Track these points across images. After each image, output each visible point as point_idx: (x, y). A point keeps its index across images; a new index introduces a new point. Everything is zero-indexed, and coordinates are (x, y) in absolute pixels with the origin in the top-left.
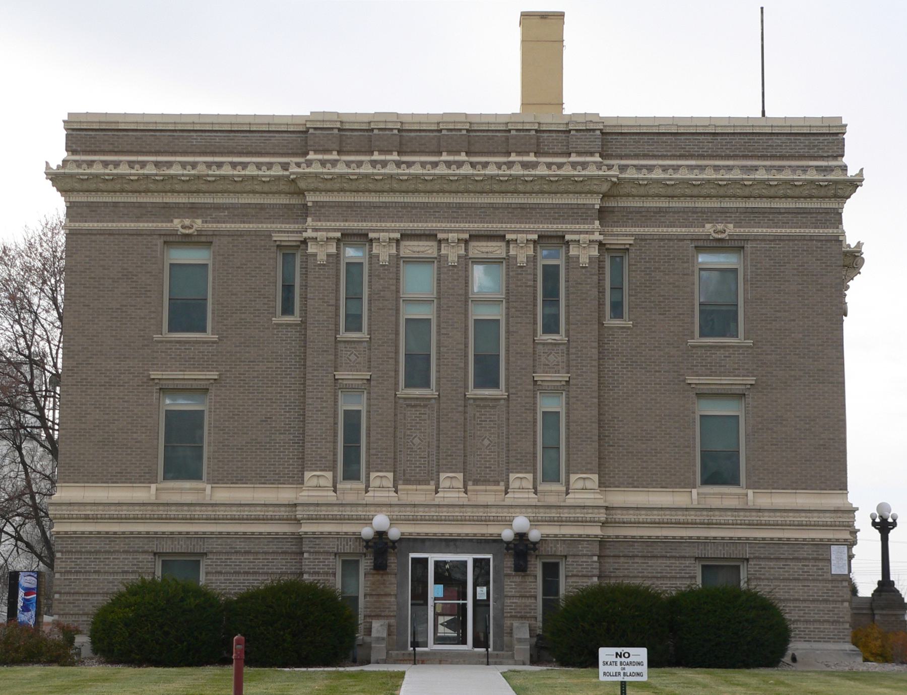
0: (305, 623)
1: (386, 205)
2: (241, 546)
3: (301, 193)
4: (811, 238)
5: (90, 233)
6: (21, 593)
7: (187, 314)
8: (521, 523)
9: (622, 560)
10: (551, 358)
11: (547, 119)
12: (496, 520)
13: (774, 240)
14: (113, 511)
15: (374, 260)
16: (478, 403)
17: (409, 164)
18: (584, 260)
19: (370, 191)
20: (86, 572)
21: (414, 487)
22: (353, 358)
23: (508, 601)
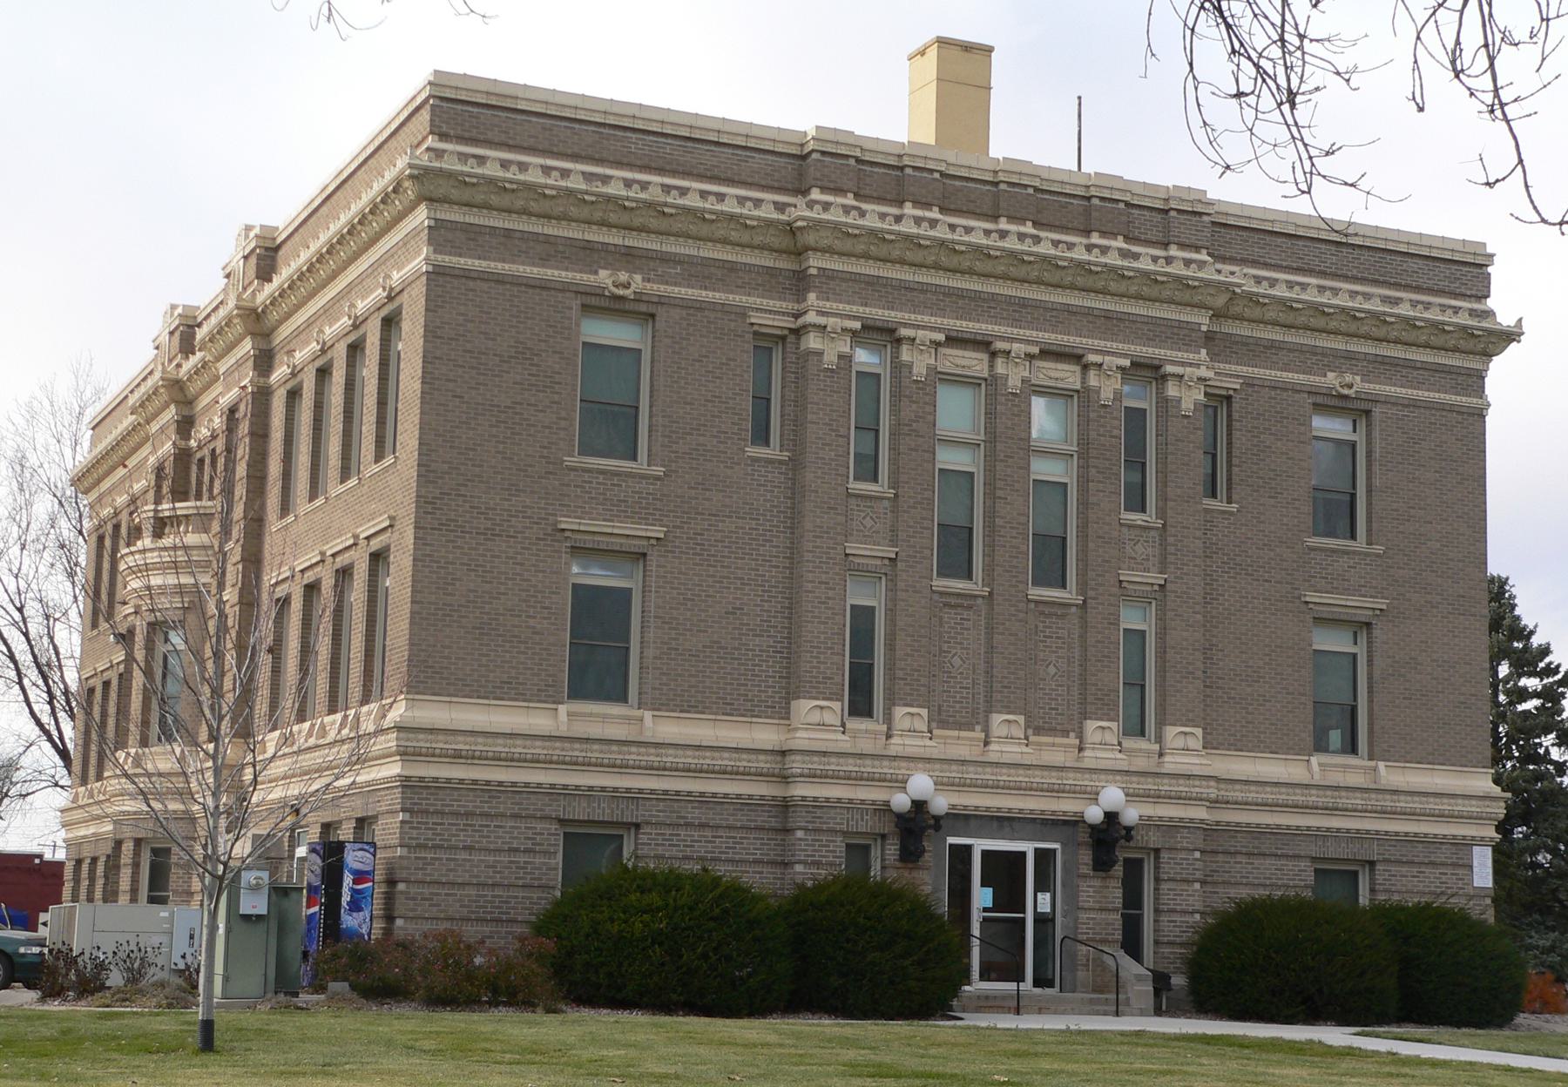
0: (865, 940)
1: (923, 289)
2: (693, 814)
3: (799, 253)
4: (1451, 409)
5: (466, 275)
6: (348, 879)
7: (612, 425)
8: (1112, 796)
9: (1221, 858)
10: (1139, 548)
11: (958, 158)
12: (1075, 792)
13: (1407, 406)
14: (500, 747)
15: (905, 371)
16: (1041, 608)
17: (1136, 256)
18: (1187, 406)
19: (490, 207)
20: (450, 848)
21: (956, 733)
22: (868, 522)
23: (1083, 916)
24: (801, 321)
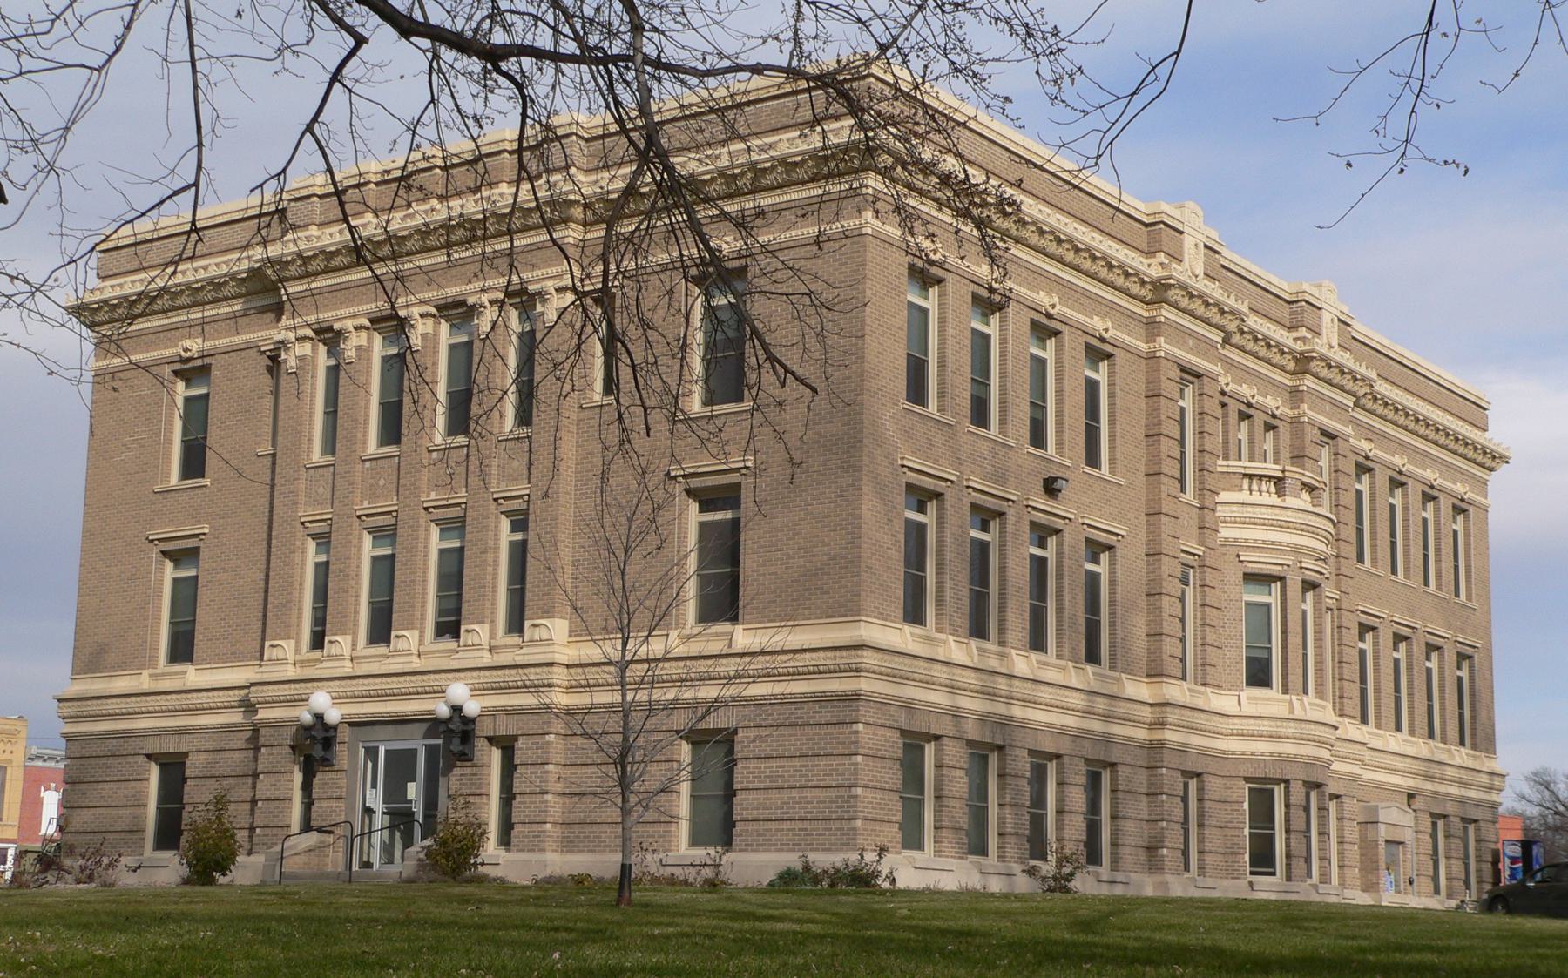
22: (321, 490)
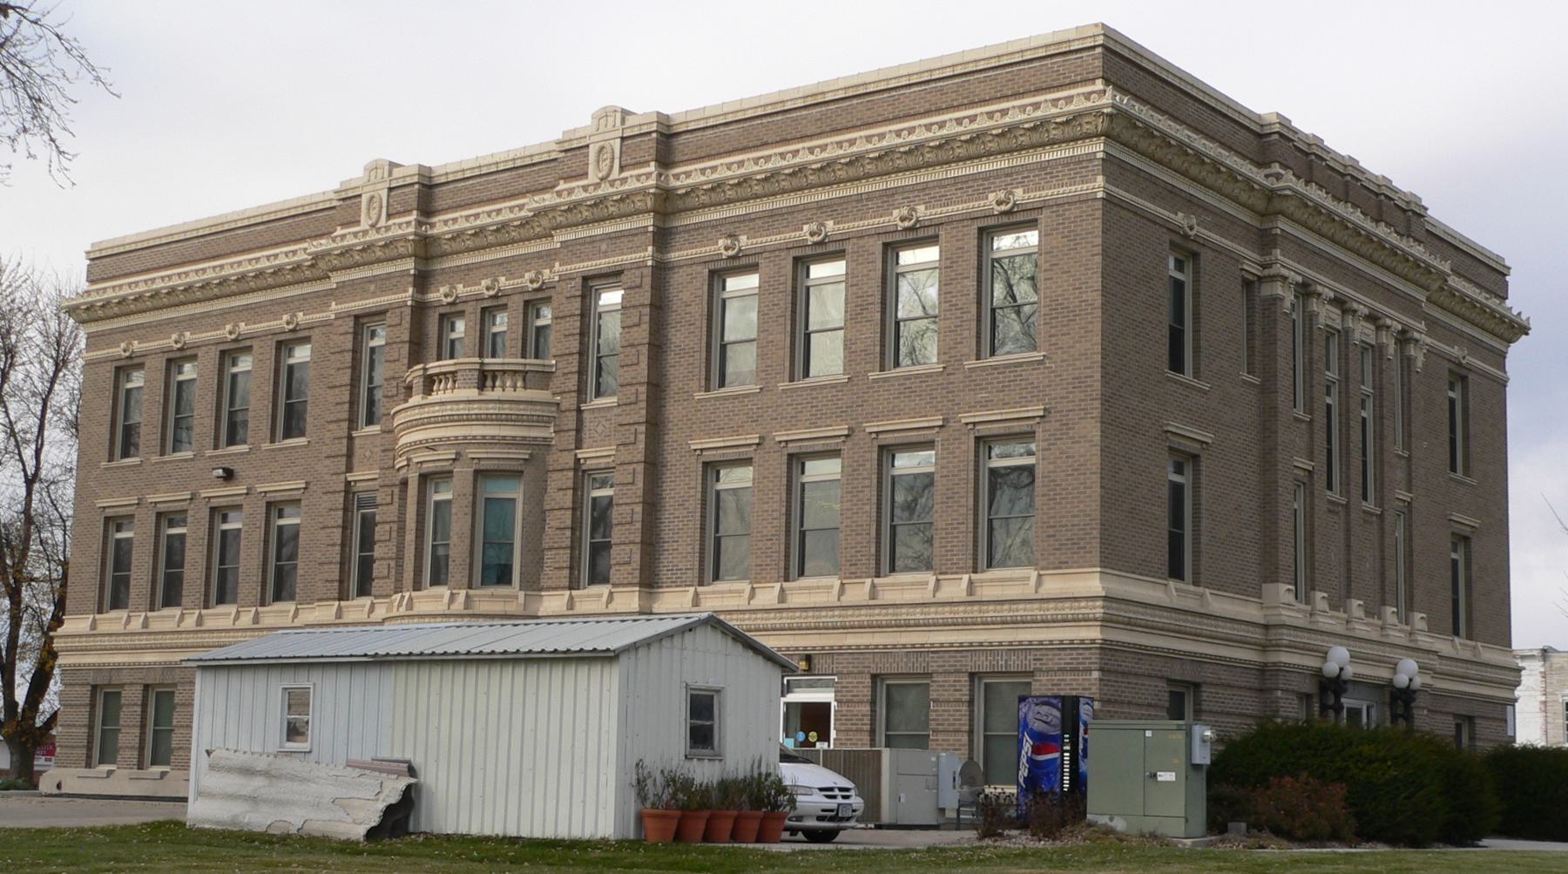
24: (1266, 272)
